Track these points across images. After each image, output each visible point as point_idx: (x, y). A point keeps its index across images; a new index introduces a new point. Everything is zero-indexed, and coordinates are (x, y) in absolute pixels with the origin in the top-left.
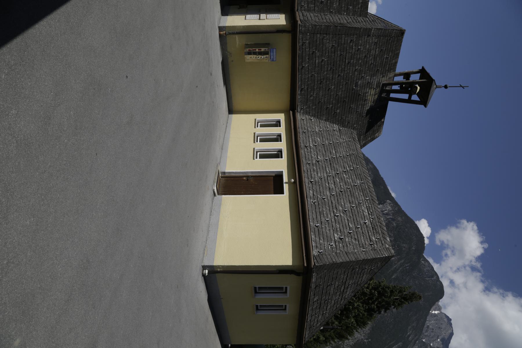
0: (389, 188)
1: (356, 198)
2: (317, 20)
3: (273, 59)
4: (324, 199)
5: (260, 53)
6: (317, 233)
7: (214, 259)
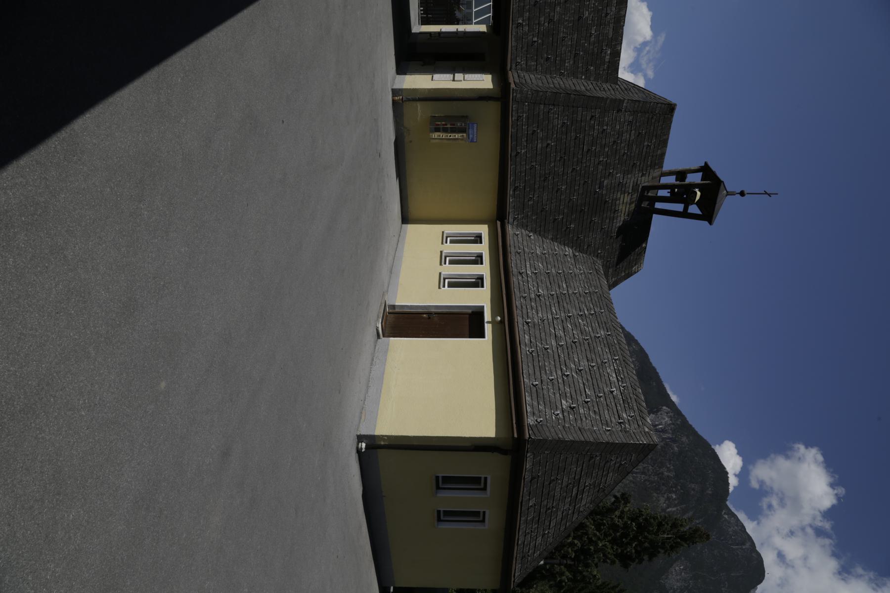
0: (667, 387)
2: (541, 84)
3: (473, 138)
4: (546, 349)
5: (453, 131)
6: (535, 395)
7: (375, 426)
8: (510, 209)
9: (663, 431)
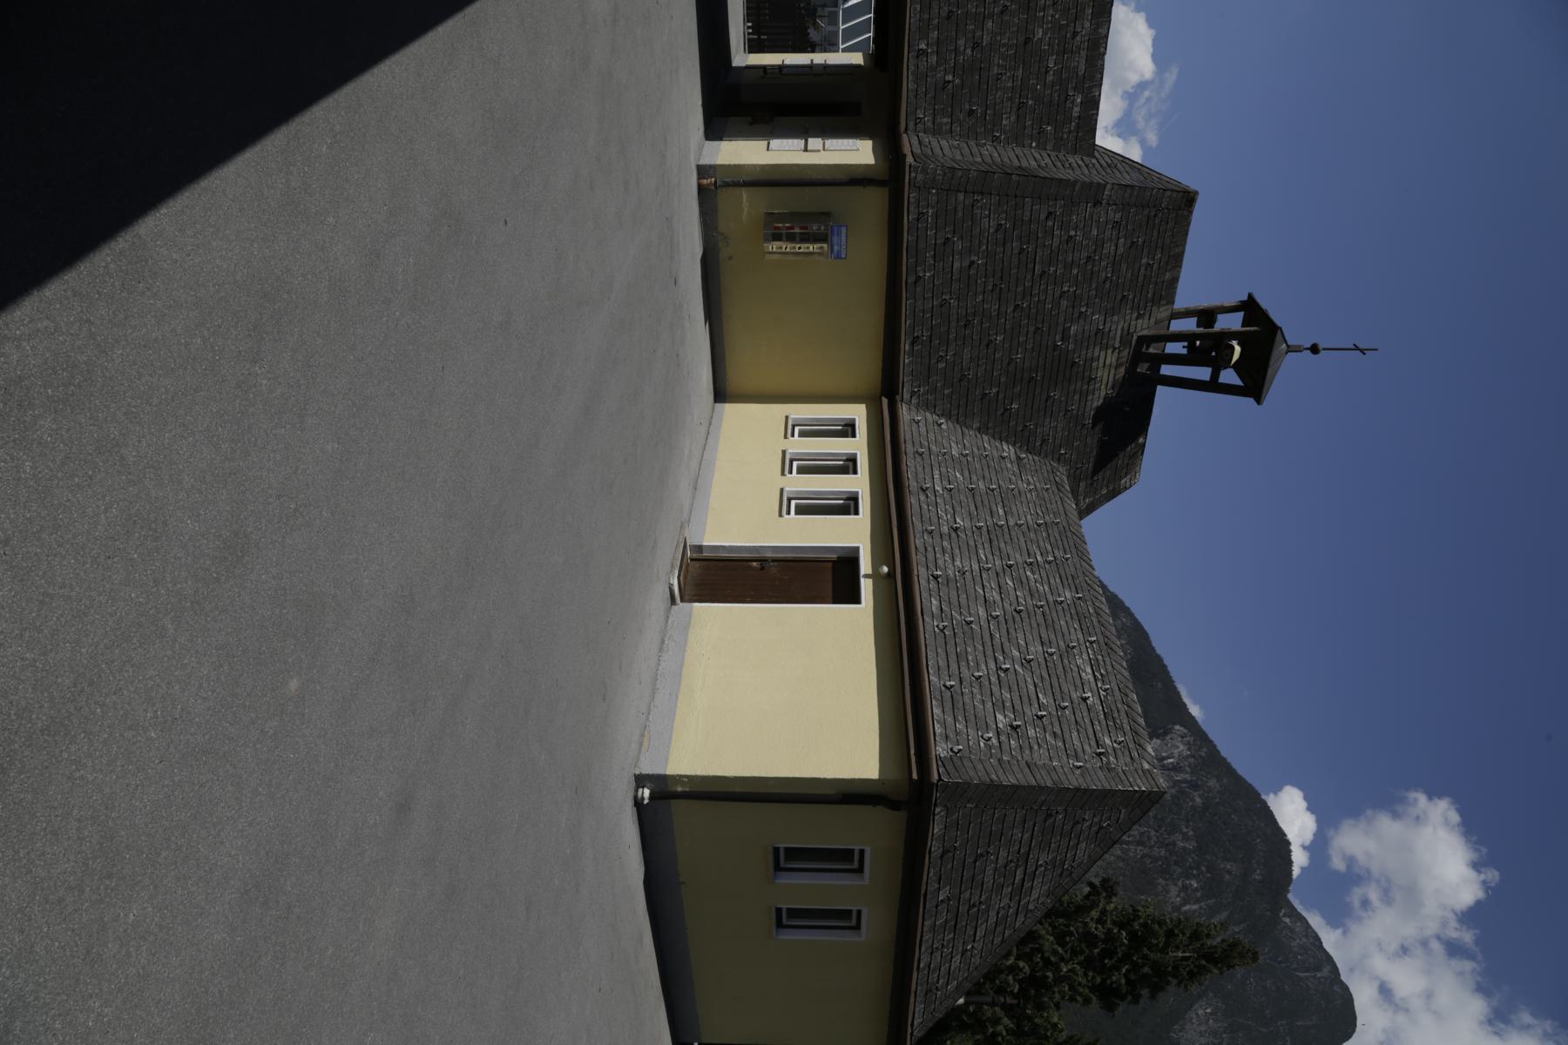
2: (959, 157)
5: (805, 238)
6: (948, 705)
9: (1176, 768)
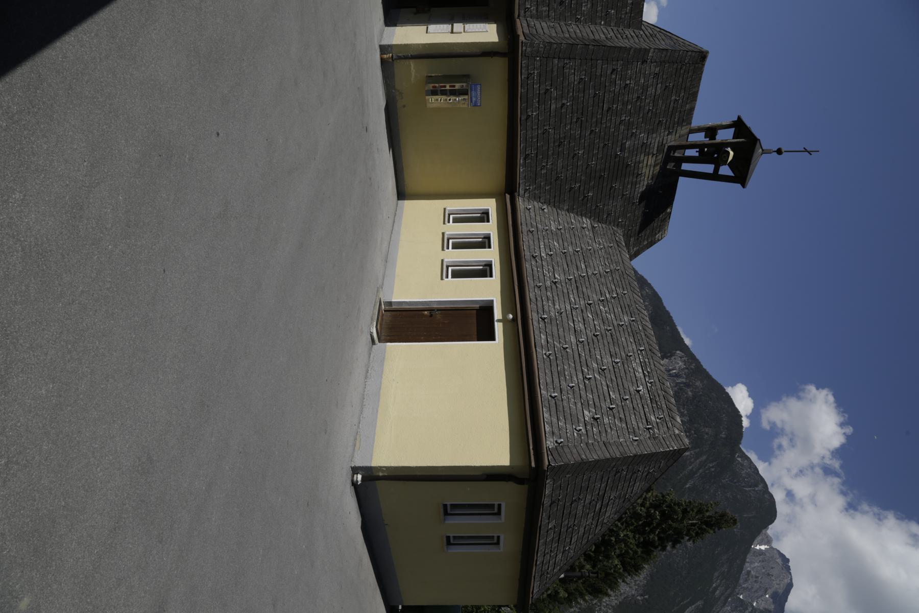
0: (680, 329)
1: (621, 347)
2: (554, 34)
3: (476, 102)
5: (453, 93)
6: (553, 409)
7: (372, 456)
8: (520, 180)
9: (677, 376)
